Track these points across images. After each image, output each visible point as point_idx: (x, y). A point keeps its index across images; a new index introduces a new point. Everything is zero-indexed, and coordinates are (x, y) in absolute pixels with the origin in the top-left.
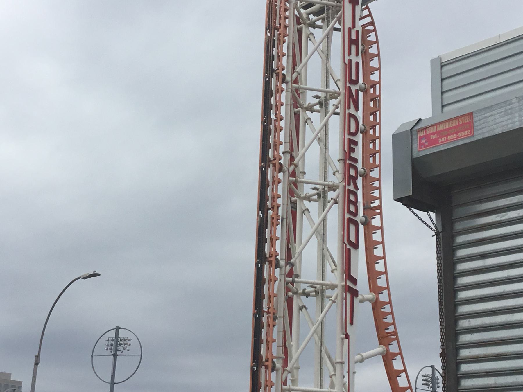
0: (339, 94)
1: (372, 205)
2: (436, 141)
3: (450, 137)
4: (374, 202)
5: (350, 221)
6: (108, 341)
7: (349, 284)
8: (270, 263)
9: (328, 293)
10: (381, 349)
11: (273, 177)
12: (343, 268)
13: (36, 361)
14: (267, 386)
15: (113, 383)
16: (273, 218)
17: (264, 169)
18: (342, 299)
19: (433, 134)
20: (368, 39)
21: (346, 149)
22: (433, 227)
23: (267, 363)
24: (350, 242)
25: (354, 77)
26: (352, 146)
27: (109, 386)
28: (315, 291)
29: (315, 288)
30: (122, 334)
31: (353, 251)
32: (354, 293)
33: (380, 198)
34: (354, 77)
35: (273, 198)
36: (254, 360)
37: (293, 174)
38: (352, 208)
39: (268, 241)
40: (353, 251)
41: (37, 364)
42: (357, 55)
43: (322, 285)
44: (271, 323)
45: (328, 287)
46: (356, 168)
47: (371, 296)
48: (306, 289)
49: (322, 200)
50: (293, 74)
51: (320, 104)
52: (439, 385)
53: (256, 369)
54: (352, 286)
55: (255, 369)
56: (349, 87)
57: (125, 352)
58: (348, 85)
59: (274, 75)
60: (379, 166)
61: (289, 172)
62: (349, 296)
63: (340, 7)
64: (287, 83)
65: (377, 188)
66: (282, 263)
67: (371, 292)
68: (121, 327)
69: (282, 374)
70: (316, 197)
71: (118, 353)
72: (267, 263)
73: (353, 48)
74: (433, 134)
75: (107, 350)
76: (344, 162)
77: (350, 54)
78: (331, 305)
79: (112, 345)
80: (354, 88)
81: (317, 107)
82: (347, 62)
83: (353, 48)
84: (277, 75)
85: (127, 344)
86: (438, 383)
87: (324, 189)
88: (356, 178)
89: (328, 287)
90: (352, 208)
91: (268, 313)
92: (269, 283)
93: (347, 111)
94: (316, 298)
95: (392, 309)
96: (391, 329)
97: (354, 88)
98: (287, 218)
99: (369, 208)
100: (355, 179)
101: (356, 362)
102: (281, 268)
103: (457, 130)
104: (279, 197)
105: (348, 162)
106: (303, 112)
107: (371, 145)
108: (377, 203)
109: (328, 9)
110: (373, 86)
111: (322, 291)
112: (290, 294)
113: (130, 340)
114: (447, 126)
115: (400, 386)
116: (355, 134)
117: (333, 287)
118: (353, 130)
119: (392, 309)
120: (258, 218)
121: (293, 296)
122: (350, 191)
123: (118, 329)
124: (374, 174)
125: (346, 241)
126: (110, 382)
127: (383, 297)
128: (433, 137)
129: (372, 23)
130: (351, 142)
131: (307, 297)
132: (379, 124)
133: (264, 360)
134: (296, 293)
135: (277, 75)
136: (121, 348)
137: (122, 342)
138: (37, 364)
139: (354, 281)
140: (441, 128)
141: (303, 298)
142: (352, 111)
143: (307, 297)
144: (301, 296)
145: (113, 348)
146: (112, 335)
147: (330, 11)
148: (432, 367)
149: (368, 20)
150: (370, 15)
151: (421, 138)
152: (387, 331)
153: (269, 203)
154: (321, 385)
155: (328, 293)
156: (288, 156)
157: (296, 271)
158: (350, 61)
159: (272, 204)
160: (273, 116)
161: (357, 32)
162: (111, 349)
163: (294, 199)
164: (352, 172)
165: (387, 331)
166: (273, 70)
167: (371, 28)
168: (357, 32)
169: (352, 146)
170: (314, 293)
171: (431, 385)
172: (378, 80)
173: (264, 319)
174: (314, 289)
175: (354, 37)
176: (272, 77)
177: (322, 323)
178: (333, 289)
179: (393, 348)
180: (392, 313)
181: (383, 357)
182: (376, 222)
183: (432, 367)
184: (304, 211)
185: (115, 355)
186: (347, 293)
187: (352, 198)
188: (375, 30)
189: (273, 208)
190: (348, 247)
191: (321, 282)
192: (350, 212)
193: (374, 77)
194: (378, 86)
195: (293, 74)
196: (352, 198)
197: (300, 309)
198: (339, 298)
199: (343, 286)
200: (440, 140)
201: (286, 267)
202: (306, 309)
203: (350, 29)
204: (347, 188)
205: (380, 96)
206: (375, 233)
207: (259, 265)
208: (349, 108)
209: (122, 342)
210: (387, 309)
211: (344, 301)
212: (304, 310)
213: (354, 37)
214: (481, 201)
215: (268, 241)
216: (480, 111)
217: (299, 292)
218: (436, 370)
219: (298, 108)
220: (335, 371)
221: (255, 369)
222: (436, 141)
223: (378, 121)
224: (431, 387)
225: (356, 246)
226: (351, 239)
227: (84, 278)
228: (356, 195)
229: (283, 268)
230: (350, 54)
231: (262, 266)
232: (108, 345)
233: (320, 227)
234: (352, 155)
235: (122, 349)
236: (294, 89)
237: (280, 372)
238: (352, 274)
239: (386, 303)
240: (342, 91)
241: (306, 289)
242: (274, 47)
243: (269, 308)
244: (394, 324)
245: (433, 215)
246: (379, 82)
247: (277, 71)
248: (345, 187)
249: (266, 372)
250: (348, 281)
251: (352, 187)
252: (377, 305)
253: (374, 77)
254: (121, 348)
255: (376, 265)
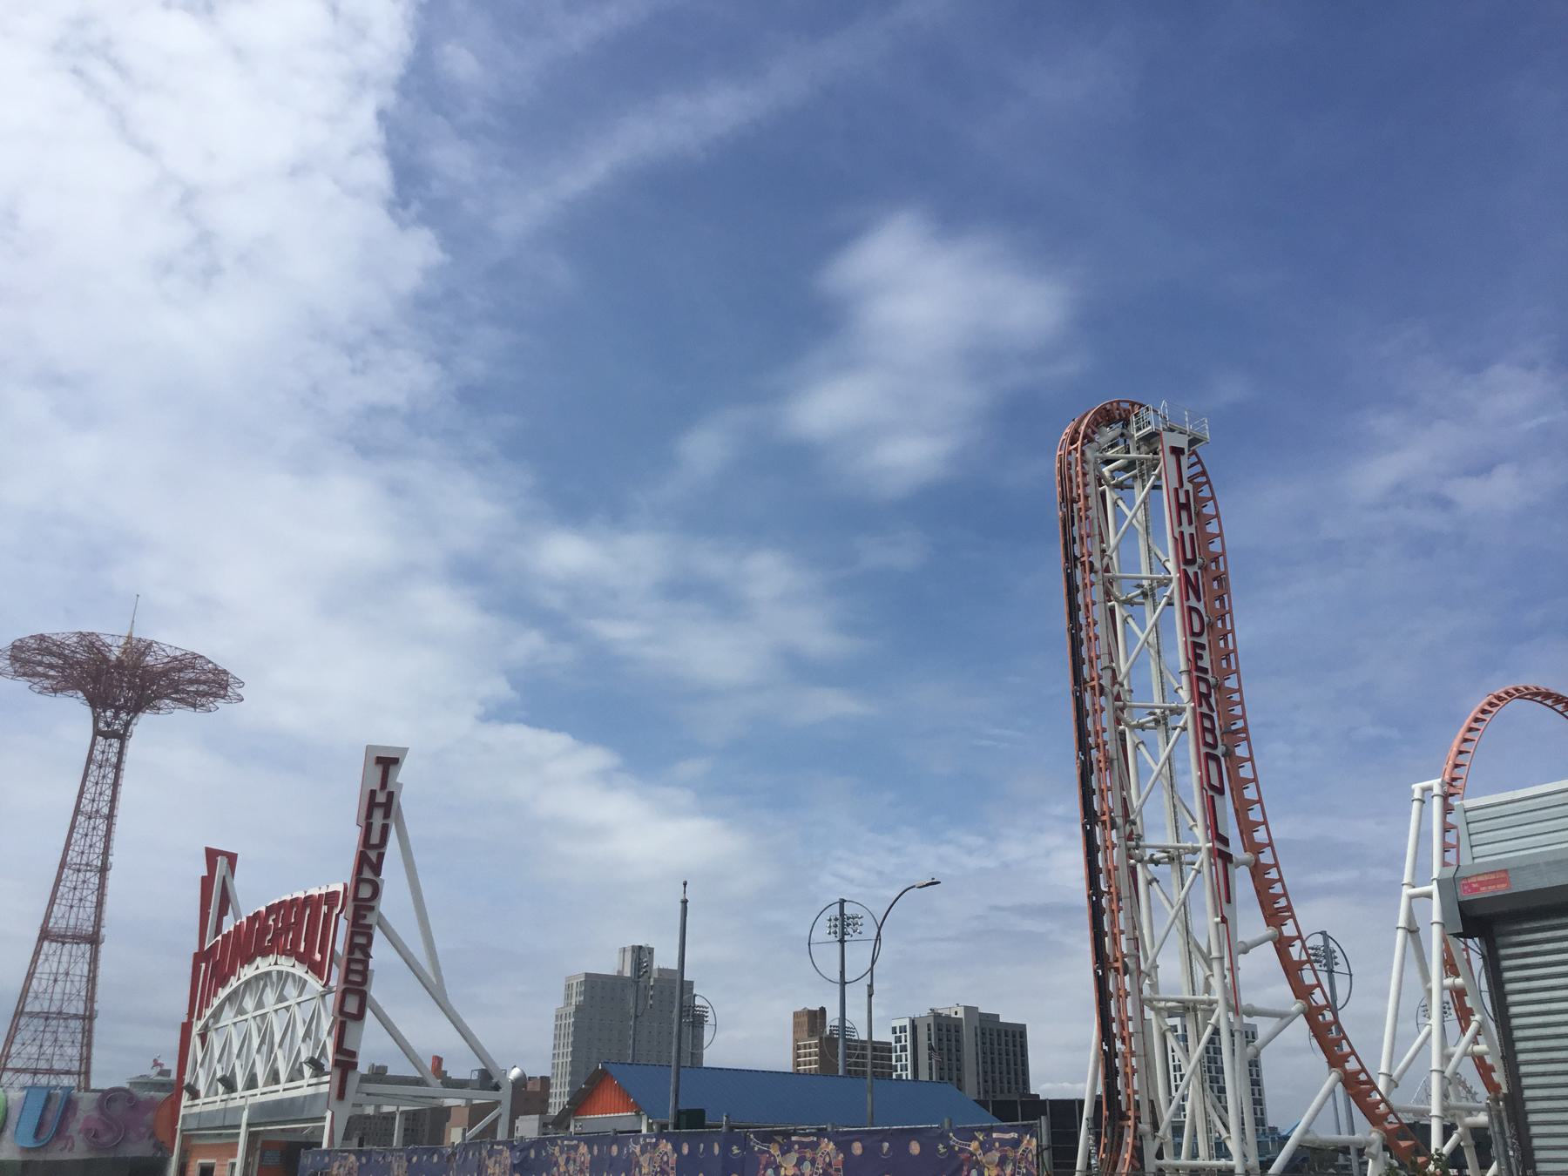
0: (1170, 580)
1: (1233, 728)
2: (1476, 890)
3: (1490, 888)
4: (1235, 724)
5: (1209, 756)
6: (830, 920)
7: (1219, 845)
8: (1104, 823)
9: (1187, 858)
10: (1271, 931)
11: (1094, 704)
12: (1206, 821)
13: (869, 992)
14: (1121, 996)
15: (843, 983)
16: (1100, 761)
17: (1078, 694)
18: (1211, 865)
19: (1474, 883)
20: (1200, 495)
21: (1190, 657)
22: (1478, 950)
23: (1116, 965)
24: (1212, 787)
25: (1189, 556)
26: (1198, 651)
27: (838, 987)
28: (1168, 857)
29: (1168, 852)
30: (849, 910)
31: (1217, 798)
32: (1226, 858)
33: (1243, 717)
34: (1189, 556)
35: (1097, 733)
36: (1097, 960)
37: (1118, 698)
38: (1209, 739)
39: (1097, 792)
40: (1217, 798)
41: (870, 996)
42: (1190, 523)
43: (1177, 849)
44: (1114, 907)
45: (1187, 851)
46: (1206, 681)
47: (1247, 856)
48: (1153, 855)
49: (1162, 728)
50: (1102, 560)
51: (1145, 595)
52: (1336, 960)
53: (1102, 972)
54: (1223, 848)
55: (1100, 973)
56: (1185, 570)
57: (856, 936)
58: (1183, 567)
59: (1079, 565)
60: (1237, 671)
61: (1113, 694)
62: (1219, 862)
63: (1159, 460)
64: (1096, 572)
65: (1238, 703)
66: (1119, 821)
67: (1245, 851)
68: (129, 630)
69: (1138, 979)
70: (1153, 724)
71: (846, 938)
72: (1100, 823)
73: (1184, 515)
74: (1474, 883)
75: (830, 933)
76: (1189, 674)
77: (1180, 524)
78: (1195, 876)
79: (836, 926)
80: (1191, 571)
81: (1140, 600)
82: (1177, 536)
83: (1184, 515)
84: (1083, 564)
85: (857, 924)
86: (1336, 957)
87: (1163, 713)
88: (1209, 695)
89: (1187, 851)
90: (1209, 739)
91: (1109, 893)
92: (1105, 852)
93: (1186, 604)
94: (1169, 866)
95: (1279, 873)
96: (1283, 902)
97: (1191, 571)
98: (1118, 759)
99: (1229, 732)
100: (1208, 696)
101: (1239, 953)
102: (1117, 829)
103: (1495, 882)
104: (1104, 730)
105: (1195, 674)
106: (1119, 606)
107: (1222, 643)
108: (1240, 724)
109: (1142, 464)
110: (1216, 560)
111: (1179, 856)
112: (1132, 861)
113: (861, 917)
114: (1486, 878)
115: (1306, 983)
116: (1200, 634)
117: (1195, 851)
118: (1197, 629)
119: (1279, 873)
120: (1079, 761)
121: (1135, 865)
122: (1203, 715)
123: (842, 902)
124: (1231, 683)
125: (1205, 786)
126: (839, 981)
127: (1266, 858)
128: (1474, 886)
129: (1204, 473)
130: (1196, 645)
131: (1156, 865)
132: (1230, 612)
133: (1111, 959)
134: (1141, 861)
135: (1083, 564)
136: (850, 930)
137: (850, 921)
138: (870, 996)
139: (1225, 841)
140: (1480, 879)
141: (1151, 866)
142: (1193, 602)
143: (1156, 865)
144: (1148, 865)
145: (838, 930)
146: (835, 910)
147: (1144, 467)
148: (1323, 933)
149: (1198, 469)
150: (1199, 462)
151: (1463, 885)
152: (1276, 906)
153: (1091, 740)
154: (1193, 990)
155: (1187, 858)
156: (1109, 672)
157: (1138, 829)
158: (1182, 533)
159: (1096, 741)
160: (1083, 621)
161: (1187, 492)
162: (836, 933)
163: (1121, 727)
164: (1203, 688)
165: (1276, 906)
166: (1076, 558)
167: (1203, 479)
168: (1187, 492)
169: (1198, 651)
170: (1167, 860)
171: (1324, 961)
172: (1220, 551)
173: (1104, 902)
174: (1165, 855)
175: (1183, 500)
176: (1076, 566)
177: (1184, 904)
178: (1194, 853)
179: (1289, 930)
180: (1281, 880)
181: (1275, 944)
182: (1241, 751)
183: (1323, 933)
184: (1138, 744)
185: (842, 941)
186: (1217, 859)
187: (1207, 724)
188: (1208, 482)
189: (1098, 746)
190: (1210, 793)
191: (1176, 844)
192: (1206, 744)
193: (1215, 547)
194: (1221, 559)
195: (1102, 560)
196: (1207, 724)
197: (1149, 883)
198: (1205, 865)
199: (1209, 849)
200: (1481, 889)
201: (1124, 827)
202: (1158, 882)
203: (1176, 490)
204: (1198, 710)
205: (1225, 573)
206: (1243, 766)
207: (1088, 827)
208: (1188, 599)
209: (850, 921)
210: (1273, 874)
211: (1214, 868)
212: (1155, 884)
213: (1183, 500)
214: (1519, 933)
215: (1097, 792)
216: (1514, 869)
217: (1145, 859)
218: (1330, 940)
219: (1111, 601)
220: (1211, 970)
221: (1100, 973)
222: (1476, 890)
223: (1227, 608)
224: (1325, 965)
225: (1221, 791)
226: (1212, 782)
227: (920, 887)
228: (1211, 718)
229: (1122, 829)
230: (1180, 524)
231: (1092, 829)
232: (830, 927)
233: (1164, 769)
234: (1200, 663)
235: (851, 932)
236: (1106, 579)
237: (1135, 974)
238: (1221, 831)
239: (1270, 867)
240: (1174, 575)
241: (1153, 855)
242: (1073, 525)
243: (1110, 887)
244: (1285, 895)
245: (1477, 939)
246: (1223, 554)
247: (1082, 559)
248: (1194, 709)
249: (1116, 977)
250: (1215, 842)
251: (1205, 709)
252: (1258, 871)
253: (1215, 547)
254: (850, 930)
255: (1250, 812)
